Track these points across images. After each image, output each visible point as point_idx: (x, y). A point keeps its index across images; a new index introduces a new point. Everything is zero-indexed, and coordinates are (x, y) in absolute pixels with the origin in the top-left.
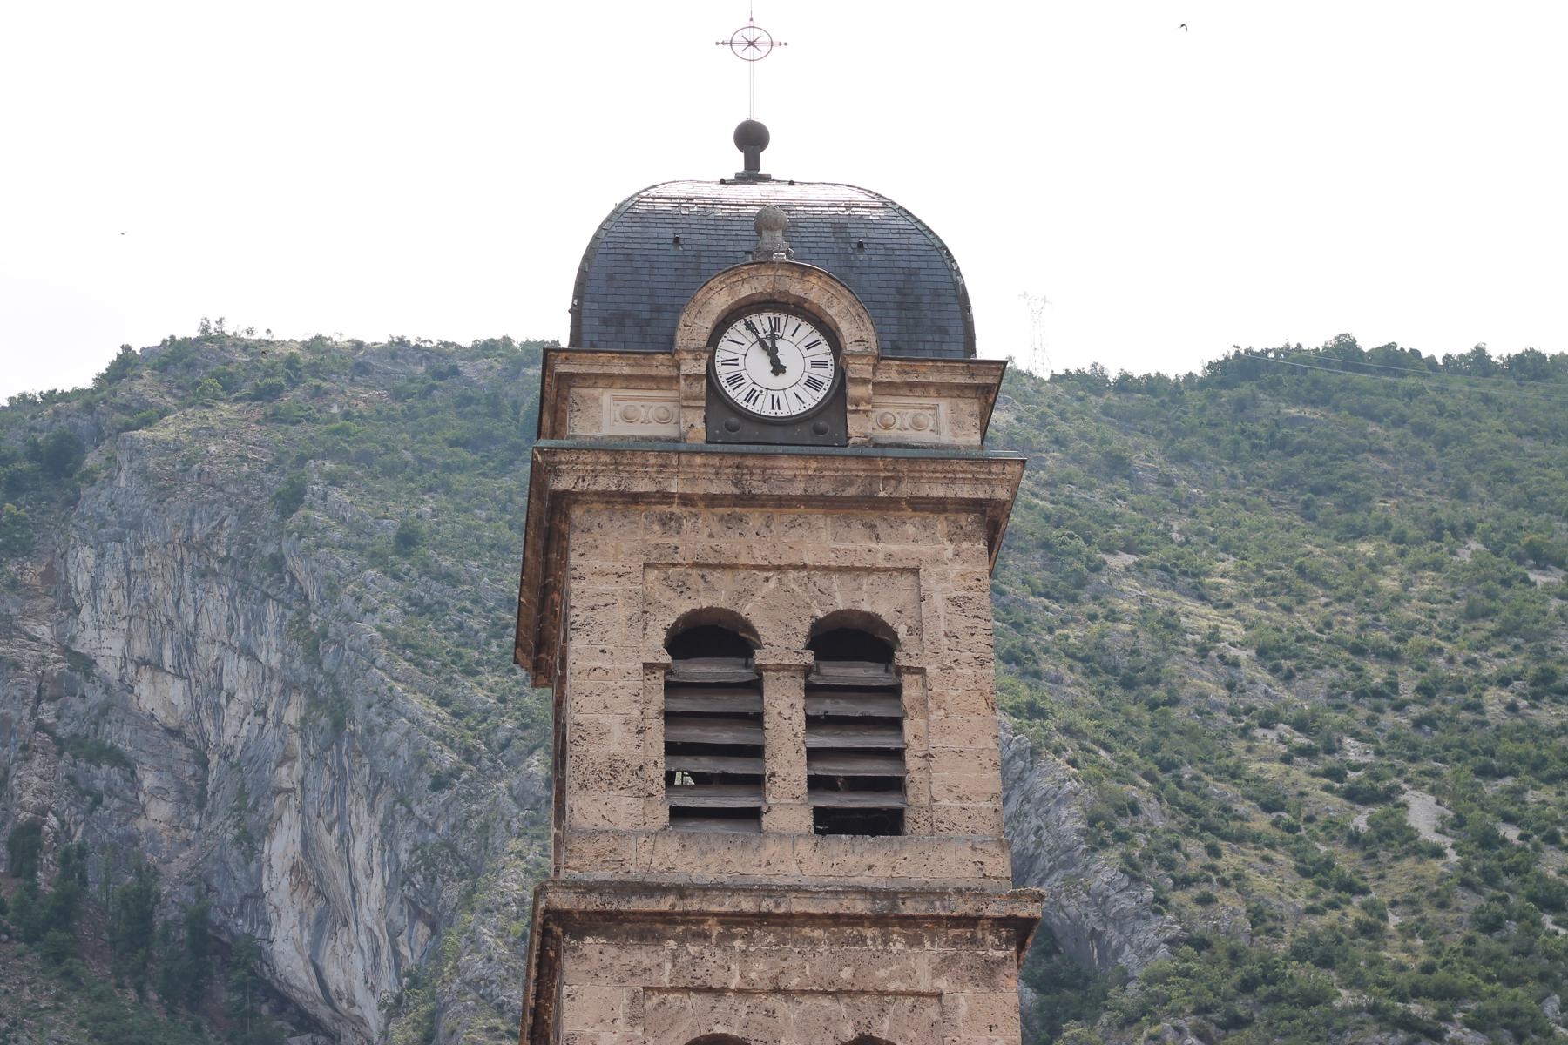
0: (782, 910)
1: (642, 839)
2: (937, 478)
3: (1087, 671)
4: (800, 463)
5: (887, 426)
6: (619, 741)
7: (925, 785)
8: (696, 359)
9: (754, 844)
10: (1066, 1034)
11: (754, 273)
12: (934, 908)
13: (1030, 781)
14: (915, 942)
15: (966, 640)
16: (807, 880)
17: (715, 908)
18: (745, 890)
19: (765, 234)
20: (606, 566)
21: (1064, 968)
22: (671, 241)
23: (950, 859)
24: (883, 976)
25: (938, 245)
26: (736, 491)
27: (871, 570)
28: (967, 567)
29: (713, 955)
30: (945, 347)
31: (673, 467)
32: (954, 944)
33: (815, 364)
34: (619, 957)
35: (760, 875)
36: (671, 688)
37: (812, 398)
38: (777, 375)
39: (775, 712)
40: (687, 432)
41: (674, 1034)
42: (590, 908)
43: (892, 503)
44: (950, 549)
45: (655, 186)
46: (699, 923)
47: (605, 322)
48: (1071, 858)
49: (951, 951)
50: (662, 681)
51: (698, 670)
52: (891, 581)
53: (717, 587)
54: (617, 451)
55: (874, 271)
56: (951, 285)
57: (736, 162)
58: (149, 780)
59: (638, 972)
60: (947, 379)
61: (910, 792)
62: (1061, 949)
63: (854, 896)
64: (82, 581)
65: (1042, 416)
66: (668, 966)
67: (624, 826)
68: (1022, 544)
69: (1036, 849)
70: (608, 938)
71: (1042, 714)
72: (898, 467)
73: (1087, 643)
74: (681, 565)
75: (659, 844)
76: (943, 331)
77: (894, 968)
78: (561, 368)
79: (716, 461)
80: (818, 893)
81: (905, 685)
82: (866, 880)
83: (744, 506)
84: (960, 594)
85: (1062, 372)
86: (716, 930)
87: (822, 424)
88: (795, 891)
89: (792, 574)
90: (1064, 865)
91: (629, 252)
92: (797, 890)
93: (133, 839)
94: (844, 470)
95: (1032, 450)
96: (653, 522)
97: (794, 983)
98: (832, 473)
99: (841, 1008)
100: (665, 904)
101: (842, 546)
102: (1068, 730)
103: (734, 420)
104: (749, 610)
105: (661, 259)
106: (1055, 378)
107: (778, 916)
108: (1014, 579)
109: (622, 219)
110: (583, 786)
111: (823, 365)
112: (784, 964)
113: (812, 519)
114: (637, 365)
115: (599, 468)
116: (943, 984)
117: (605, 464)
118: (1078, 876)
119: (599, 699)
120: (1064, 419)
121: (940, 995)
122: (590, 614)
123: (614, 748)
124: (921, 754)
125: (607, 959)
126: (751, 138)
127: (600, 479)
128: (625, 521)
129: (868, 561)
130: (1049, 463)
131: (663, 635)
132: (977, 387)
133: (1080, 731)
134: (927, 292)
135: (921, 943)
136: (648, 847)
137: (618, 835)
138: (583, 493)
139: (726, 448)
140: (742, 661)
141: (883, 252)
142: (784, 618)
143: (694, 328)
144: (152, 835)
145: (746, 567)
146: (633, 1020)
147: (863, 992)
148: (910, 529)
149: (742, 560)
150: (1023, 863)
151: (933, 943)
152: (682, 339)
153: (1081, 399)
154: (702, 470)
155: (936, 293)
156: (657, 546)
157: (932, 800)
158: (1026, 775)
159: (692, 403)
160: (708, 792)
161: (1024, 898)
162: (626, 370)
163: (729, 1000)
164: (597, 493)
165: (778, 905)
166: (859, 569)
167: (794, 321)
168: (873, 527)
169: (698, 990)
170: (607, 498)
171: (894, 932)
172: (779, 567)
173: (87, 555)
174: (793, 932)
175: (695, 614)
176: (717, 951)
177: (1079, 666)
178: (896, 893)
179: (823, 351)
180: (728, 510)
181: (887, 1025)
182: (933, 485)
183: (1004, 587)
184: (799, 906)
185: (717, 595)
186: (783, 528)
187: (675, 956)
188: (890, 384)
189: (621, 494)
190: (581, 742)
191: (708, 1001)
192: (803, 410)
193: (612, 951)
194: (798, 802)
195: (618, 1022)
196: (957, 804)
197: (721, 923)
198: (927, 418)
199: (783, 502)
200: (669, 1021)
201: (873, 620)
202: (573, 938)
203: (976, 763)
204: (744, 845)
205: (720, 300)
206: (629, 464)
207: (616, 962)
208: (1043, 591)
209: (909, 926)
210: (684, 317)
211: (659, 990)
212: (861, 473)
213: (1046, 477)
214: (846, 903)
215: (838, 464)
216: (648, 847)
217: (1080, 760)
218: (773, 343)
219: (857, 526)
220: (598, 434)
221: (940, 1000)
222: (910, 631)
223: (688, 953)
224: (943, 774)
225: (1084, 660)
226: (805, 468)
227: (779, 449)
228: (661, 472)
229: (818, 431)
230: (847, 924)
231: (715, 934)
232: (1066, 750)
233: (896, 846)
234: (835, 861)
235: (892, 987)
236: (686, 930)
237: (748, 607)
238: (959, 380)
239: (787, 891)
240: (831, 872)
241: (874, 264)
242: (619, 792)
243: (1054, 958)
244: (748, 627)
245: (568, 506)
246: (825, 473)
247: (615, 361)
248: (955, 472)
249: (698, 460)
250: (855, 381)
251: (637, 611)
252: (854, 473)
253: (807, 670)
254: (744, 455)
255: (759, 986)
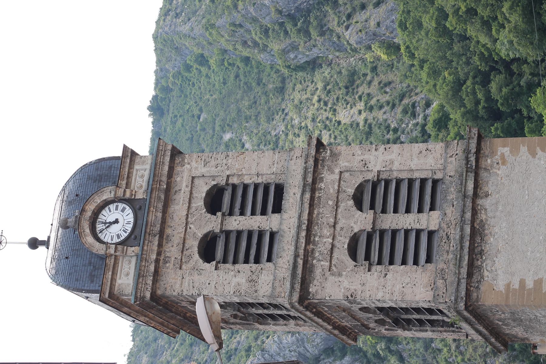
0: (306, 222)
1: (277, 271)
2: (162, 168)
3: (237, 333)
4: (151, 213)
5: (141, 186)
6: (242, 279)
7: (268, 176)
8: (110, 248)
9: (282, 233)
10: (362, 346)
11: (82, 227)
12: (311, 171)
13: (273, 353)
14: (322, 179)
15: (219, 161)
16: (297, 215)
17: (303, 245)
18: (298, 234)
19: (68, 225)
20: (179, 282)
21: (339, 345)
22: (67, 260)
23: (294, 167)
24: (332, 191)
25: (80, 169)
26: (158, 236)
27: (191, 193)
28: (194, 161)
29: (320, 247)
30: (116, 166)
31: (147, 257)
32: (324, 166)
33: (117, 209)
34: (318, 280)
35: (293, 231)
36: (225, 261)
37: (128, 210)
38: (119, 222)
39: (237, 226)
40: (135, 253)
41: (346, 261)
42: (299, 288)
43: (169, 184)
44: (187, 166)
45: (46, 269)
46: (308, 252)
47: (92, 282)
48: (301, 340)
49: (326, 168)
50: (222, 264)
51: (219, 253)
52: (196, 187)
53: (191, 245)
54: (140, 275)
55: (86, 191)
56: (95, 164)
57: (42, 249)
59: (323, 273)
60: (127, 165)
61: (270, 181)
62: (332, 346)
63: (304, 198)
65: (146, 345)
66: (322, 263)
67: (272, 277)
68: (190, 354)
69: (296, 352)
70: (310, 283)
71: (250, 347)
72: (156, 180)
73: (227, 333)
74: (182, 257)
75: (279, 265)
76: (110, 167)
77: (330, 187)
78: (107, 296)
79: (146, 242)
80: (301, 210)
81: (232, 182)
82: (298, 196)
83: (164, 235)
84: (203, 163)
85: (132, 338)
86: (311, 246)
87: (138, 207)
88: (300, 217)
89: (189, 219)
90: (303, 343)
91: (68, 274)
92: (300, 216)
94: (155, 199)
95: (157, 349)
96: (165, 266)
97: (332, 220)
98: (156, 203)
99: (342, 205)
100: (300, 262)
101: (181, 202)
102: (256, 339)
103: (133, 237)
104: (200, 235)
105: (72, 263)
106: (133, 340)
107: (308, 224)
108: (202, 357)
109: (56, 278)
110: (256, 291)
111: (117, 207)
112: (325, 223)
113: (171, 212)
114: (109, 269)
115: (144, 282)
116: (337, 171)
117: (143, 280)
118: (307, 338)
119: (226, 286)
120: (148, 337)
121: (340, 172)
122: (195, 288)
123: (244, 281)
124: (257, 177)
125: (318, 284)
126: (34, 244)
127: (148, 282)
128: (164, 276)
129: (188, 194)
130: (162, 344)
131: (206, 263)
133: (257, 334)
134: (96, 172)
135: (322, 178)
136: (280, 269)
137: (275, 279)
138: (152, 289)
139: (142, 238)
140: (218, 238)
141: (80, 188)
142: (205, 222)
143: (99, 249)
145: (185, 235)
146: (340, 275)
147: (338, 197)
148: (178, 179)
149: (182, 236)
150: (301, 357)
151: (323, 174)
152: (102, 252)
153: (142, 332)
154: (149, 247)
155: (97, 169)
156: (174, 265)
157: (273, 174)
158: (270, 354)
159: (125, 251)
160: (263, 251)
161: (310, 142)
162: (110, 273)
163: (336, 242)
164: (153, 284)
165: (304, 224)
166: (190, 197)
167: (101, 216)
168: (176, 192)
169: (332, 253)
170: (155, 280)
171: (318, 187)
172: (187, 224)
174: (314, 220)
175: (199, 253)
176: (319, 246)
177: (234, 336)
178: (304, 184)
179: (112, 207)
180: (164, 240)
181: (350, 190)
182: (164, 169)
183: (204, 360)
184: (305, 216)
185: (194, 245)
186: (173, 222)
187: (319, 260)
188: (127, 184)
189: (154, 276)
190: (240, 292)
191: (336, 250)
192: (132, 214)
193: (315, 282)
194: (269, 219)
195: (340, 280)
196: (275, 165)
197: (309, 244)
198: (140, 173)
200: (341, 263)
201: (209, 193)
202: (309, 295)
203: (262, 158)
204: (282, 236)
205: (90, 239)
206: (144, 272)
207: (319, 281)
208: (207, 347)
209: (316, 181)
210: (94, 252)
211: (330, 266)
212: (157, 193)
213: (167, 345)
214: (306, 200)
215: (153, 201)
216: (280, 269)
217: (267, 335)
218: (107, 223)
219: (175, 197)
220: (132, 284)
221: (343, 172)
222: (214, 180)
223: (318, 256)
224: (265, 170)
225: (233, 334)
226: (153, 212)
227: (145, 220)
228: (148, 261)
229: (140, 208)
230: (313, 202)
231: (312, 247)
232: (263, 340)
233: (288, 185)
234: (291, 206)
235: (336, 188)
236: (310, 256)
237: (199, 235)
238: (128, 161)
239: (300, 220)
240: (295, 207)
241: (84, 190)
242: (259, 279)
243: (335, 349)
244: (206, 236)
245: (156, 296)
246: (155, 205)
247: (107, 277)
248: (160, 162)
249: (145, 248)
250: (124, 195)
252: (156, 195)
253: (223, 215)
254: (145, 232)
255: (332, 232)
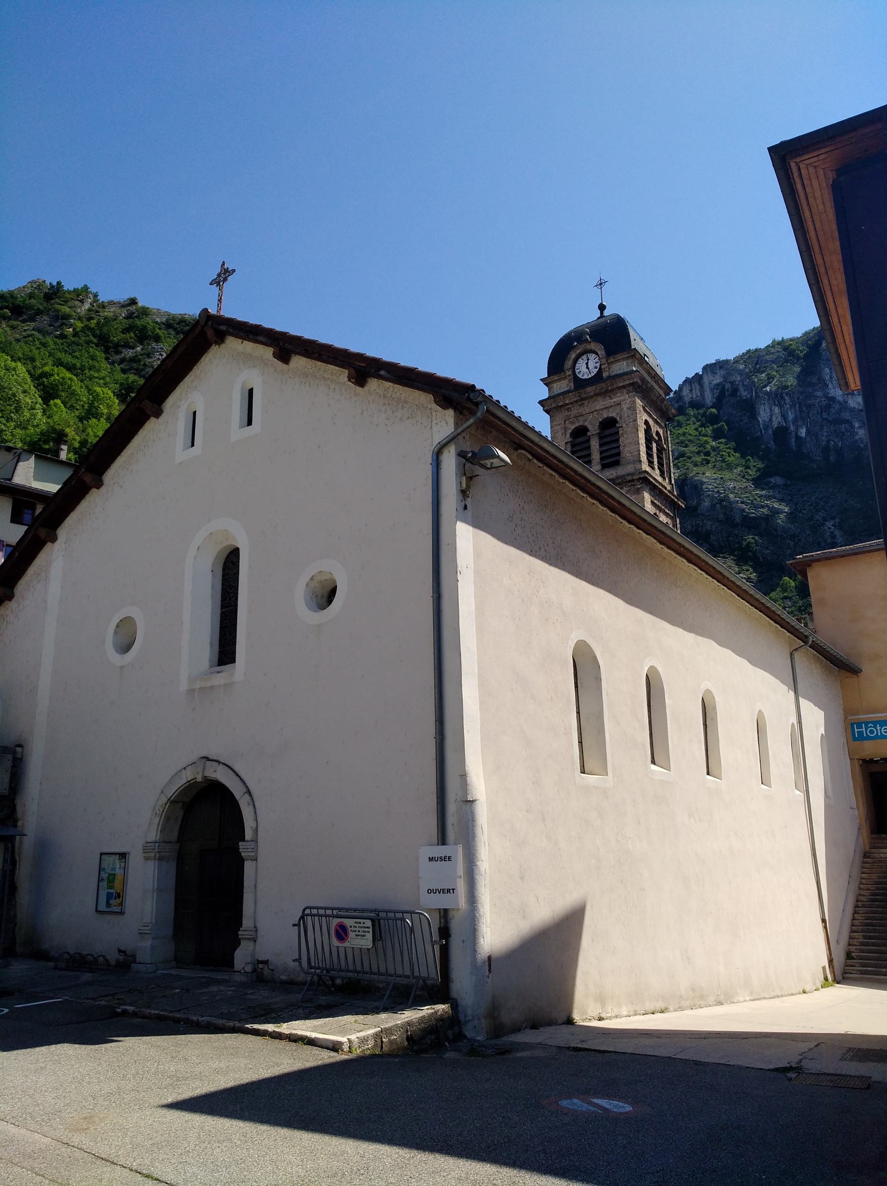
27: (611, 406)
58: (857, 425)
64: (827, 378)
89: (595, 413)
93: (856, 442)
126: (602, 307)
132: (631, 356)
144: (861, 439)
145: (585, 414)
168: (610, 397)
172: (592, 412)
173: (827, 370)
196: (630, 455)
199: (591, 397)
201: (612, 417)
251: (563, 431)
